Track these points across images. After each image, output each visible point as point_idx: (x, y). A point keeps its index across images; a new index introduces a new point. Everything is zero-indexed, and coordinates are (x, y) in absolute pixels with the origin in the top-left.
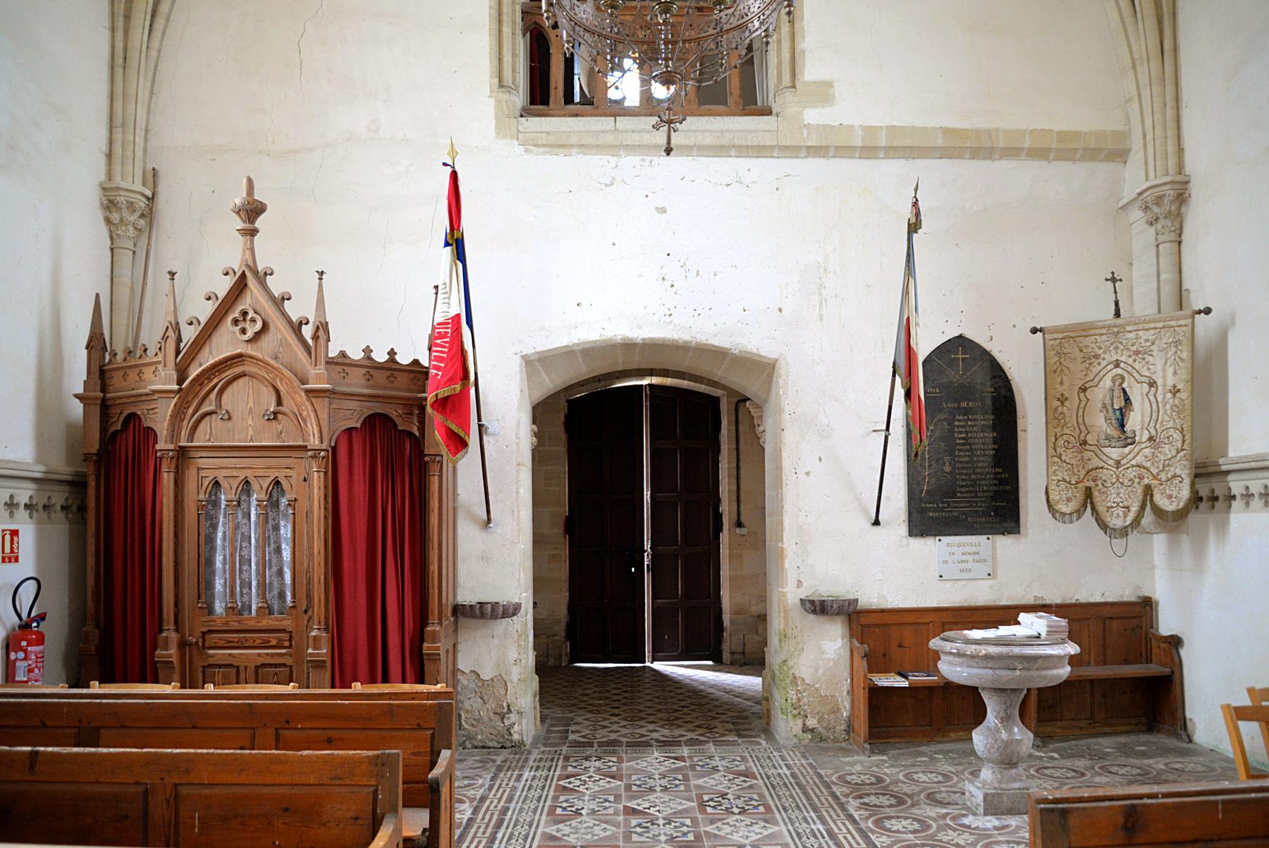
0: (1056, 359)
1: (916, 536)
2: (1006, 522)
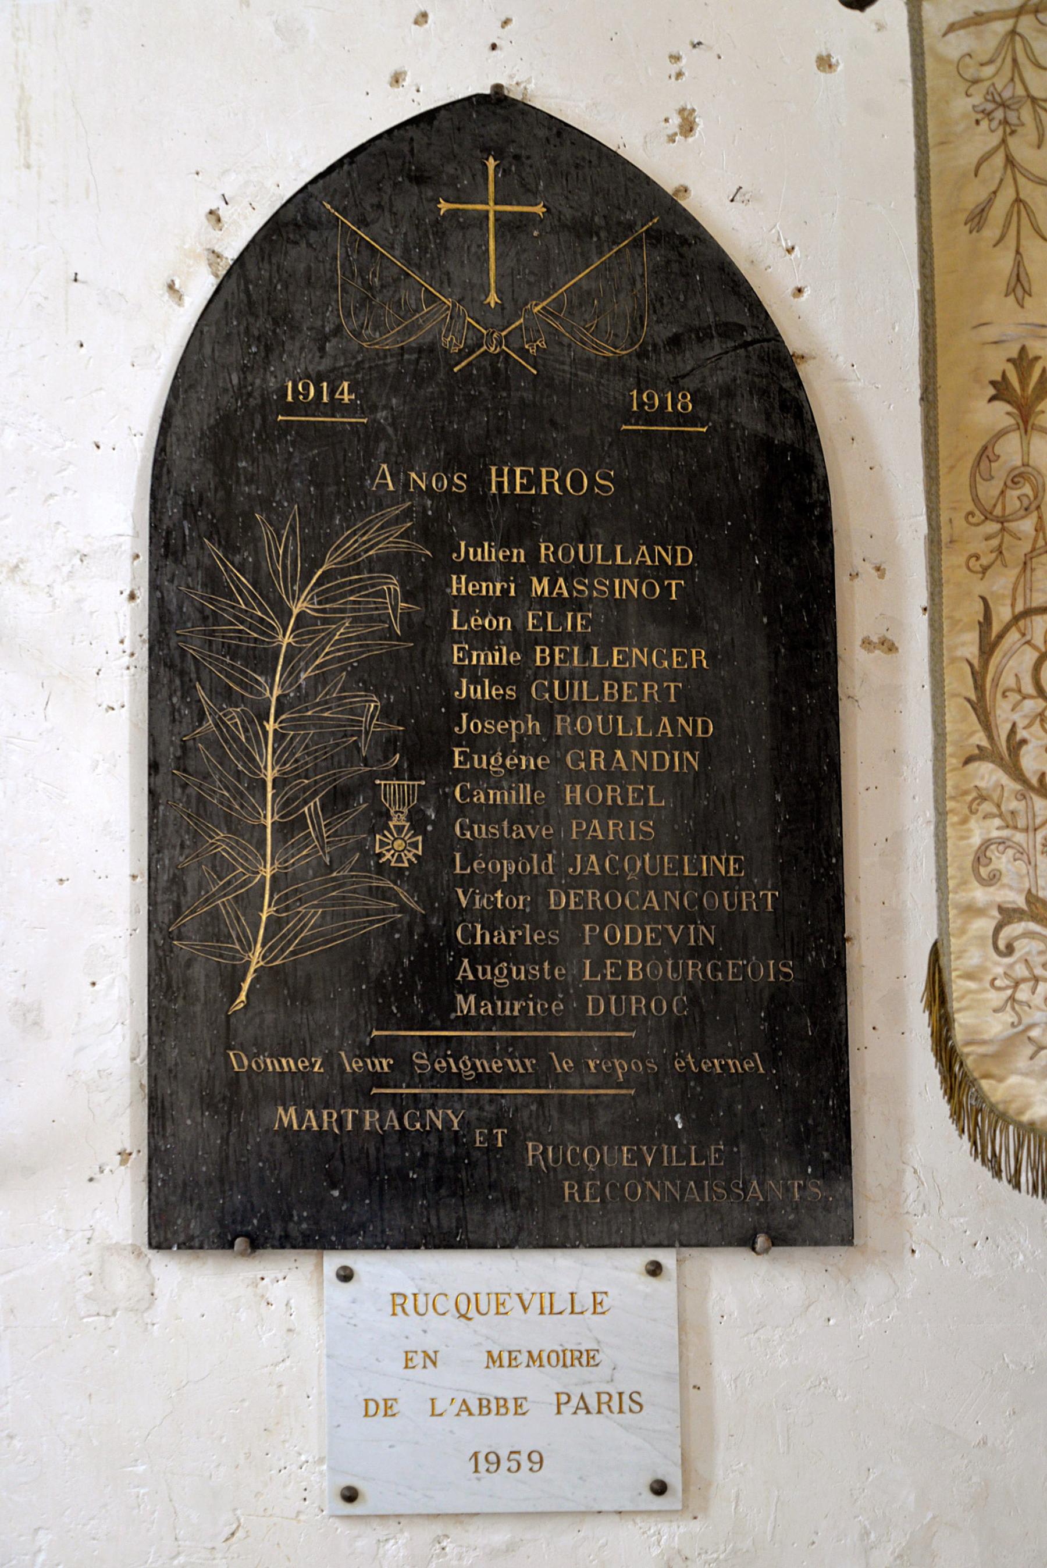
0: (985, 138)
1: (189, 1244)
2: (763, 1172)
